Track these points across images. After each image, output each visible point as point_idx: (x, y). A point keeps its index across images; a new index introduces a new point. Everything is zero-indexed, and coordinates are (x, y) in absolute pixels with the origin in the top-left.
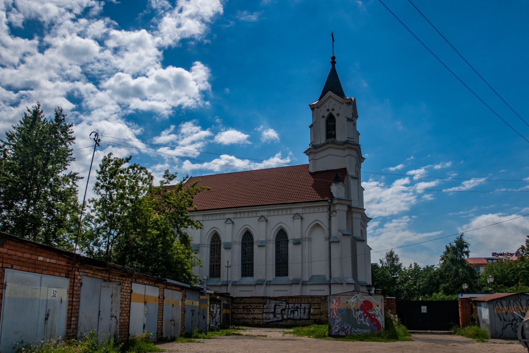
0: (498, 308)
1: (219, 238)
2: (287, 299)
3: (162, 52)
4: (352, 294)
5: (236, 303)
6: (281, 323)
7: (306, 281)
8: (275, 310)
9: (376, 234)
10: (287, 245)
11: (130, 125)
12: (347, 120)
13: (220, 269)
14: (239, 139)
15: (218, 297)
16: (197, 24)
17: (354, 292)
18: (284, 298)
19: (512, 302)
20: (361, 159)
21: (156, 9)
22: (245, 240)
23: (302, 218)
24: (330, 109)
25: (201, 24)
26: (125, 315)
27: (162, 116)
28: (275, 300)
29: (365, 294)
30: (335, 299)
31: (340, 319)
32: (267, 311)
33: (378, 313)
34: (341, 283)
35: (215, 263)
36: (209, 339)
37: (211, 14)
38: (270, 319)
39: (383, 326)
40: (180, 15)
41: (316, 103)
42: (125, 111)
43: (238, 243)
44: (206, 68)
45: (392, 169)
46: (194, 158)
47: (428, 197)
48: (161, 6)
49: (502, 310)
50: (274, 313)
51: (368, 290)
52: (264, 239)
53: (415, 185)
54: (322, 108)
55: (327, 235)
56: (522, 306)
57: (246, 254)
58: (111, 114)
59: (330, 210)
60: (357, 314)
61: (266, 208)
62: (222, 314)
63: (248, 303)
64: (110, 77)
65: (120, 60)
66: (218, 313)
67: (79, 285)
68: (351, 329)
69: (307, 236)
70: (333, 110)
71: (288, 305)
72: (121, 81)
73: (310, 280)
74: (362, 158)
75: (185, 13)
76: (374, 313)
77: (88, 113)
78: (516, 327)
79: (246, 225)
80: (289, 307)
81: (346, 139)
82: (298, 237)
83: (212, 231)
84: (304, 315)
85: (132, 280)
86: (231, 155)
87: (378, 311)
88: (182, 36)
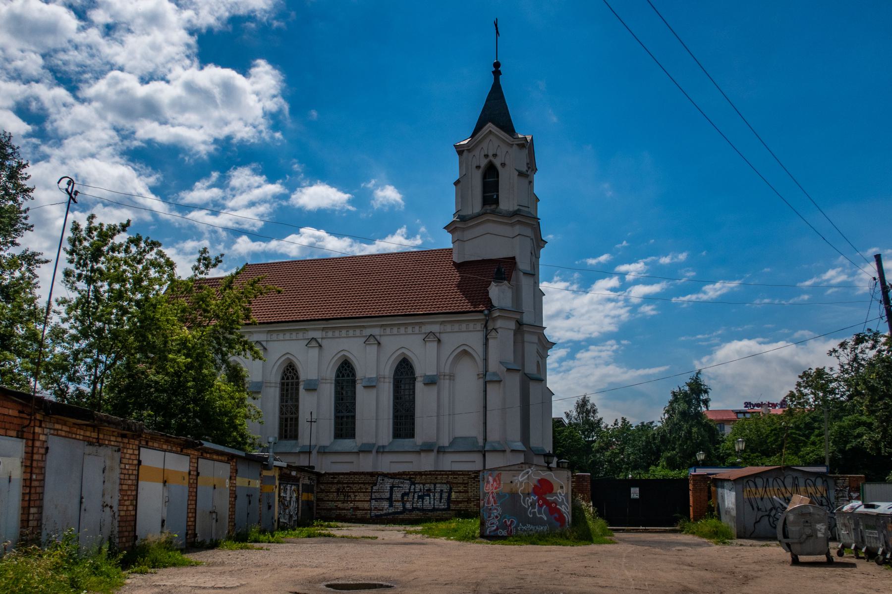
1: (296, 371)
2: (412, 477)
4: (520, 469)
5: (325, 483)
6: (401, 516)
8: (391, 494)
10: (414, 386)
12: (518, 175)
14: (334, 201)
15: (294, 473)
17: (523, 465)
18: (407, 475)
19: (771, 480)
22: (341, 376)
23: (439, 341)
24: (490, 154)
26: (127, 503)
27: (195, 154)
28: (391, 478)
29: (541, 469)
31: (499, 509)
32: (378, 496)
34: (503, 449)
35: (289, 415)
36: (278, 543)
38: (382, 510)
42: (127, 143)
43: (329, 381)
45: (592, 262)
49: (756, 493)
50: (390, 500)
53: (628, 290)
54: (477, 152)
55: (481, 369)
56: (786, 488)
57: (342, 399)
58: (101, 147)
59: (486, 328)
60: (528, 500)
62: (300, 502)
64: (97, 79)
66: (294, 499)
67: (42, 451)
68: (518, 525)
69: (447, 371)
70: (495, 155)
71: (413, 487)
76: (555, 499)
78: (775, 519)
80: (414, 489)
81: (516, 208)
82: (431, 372)
84: (440, 502)
85: (140, 443)
87: (561, 495)
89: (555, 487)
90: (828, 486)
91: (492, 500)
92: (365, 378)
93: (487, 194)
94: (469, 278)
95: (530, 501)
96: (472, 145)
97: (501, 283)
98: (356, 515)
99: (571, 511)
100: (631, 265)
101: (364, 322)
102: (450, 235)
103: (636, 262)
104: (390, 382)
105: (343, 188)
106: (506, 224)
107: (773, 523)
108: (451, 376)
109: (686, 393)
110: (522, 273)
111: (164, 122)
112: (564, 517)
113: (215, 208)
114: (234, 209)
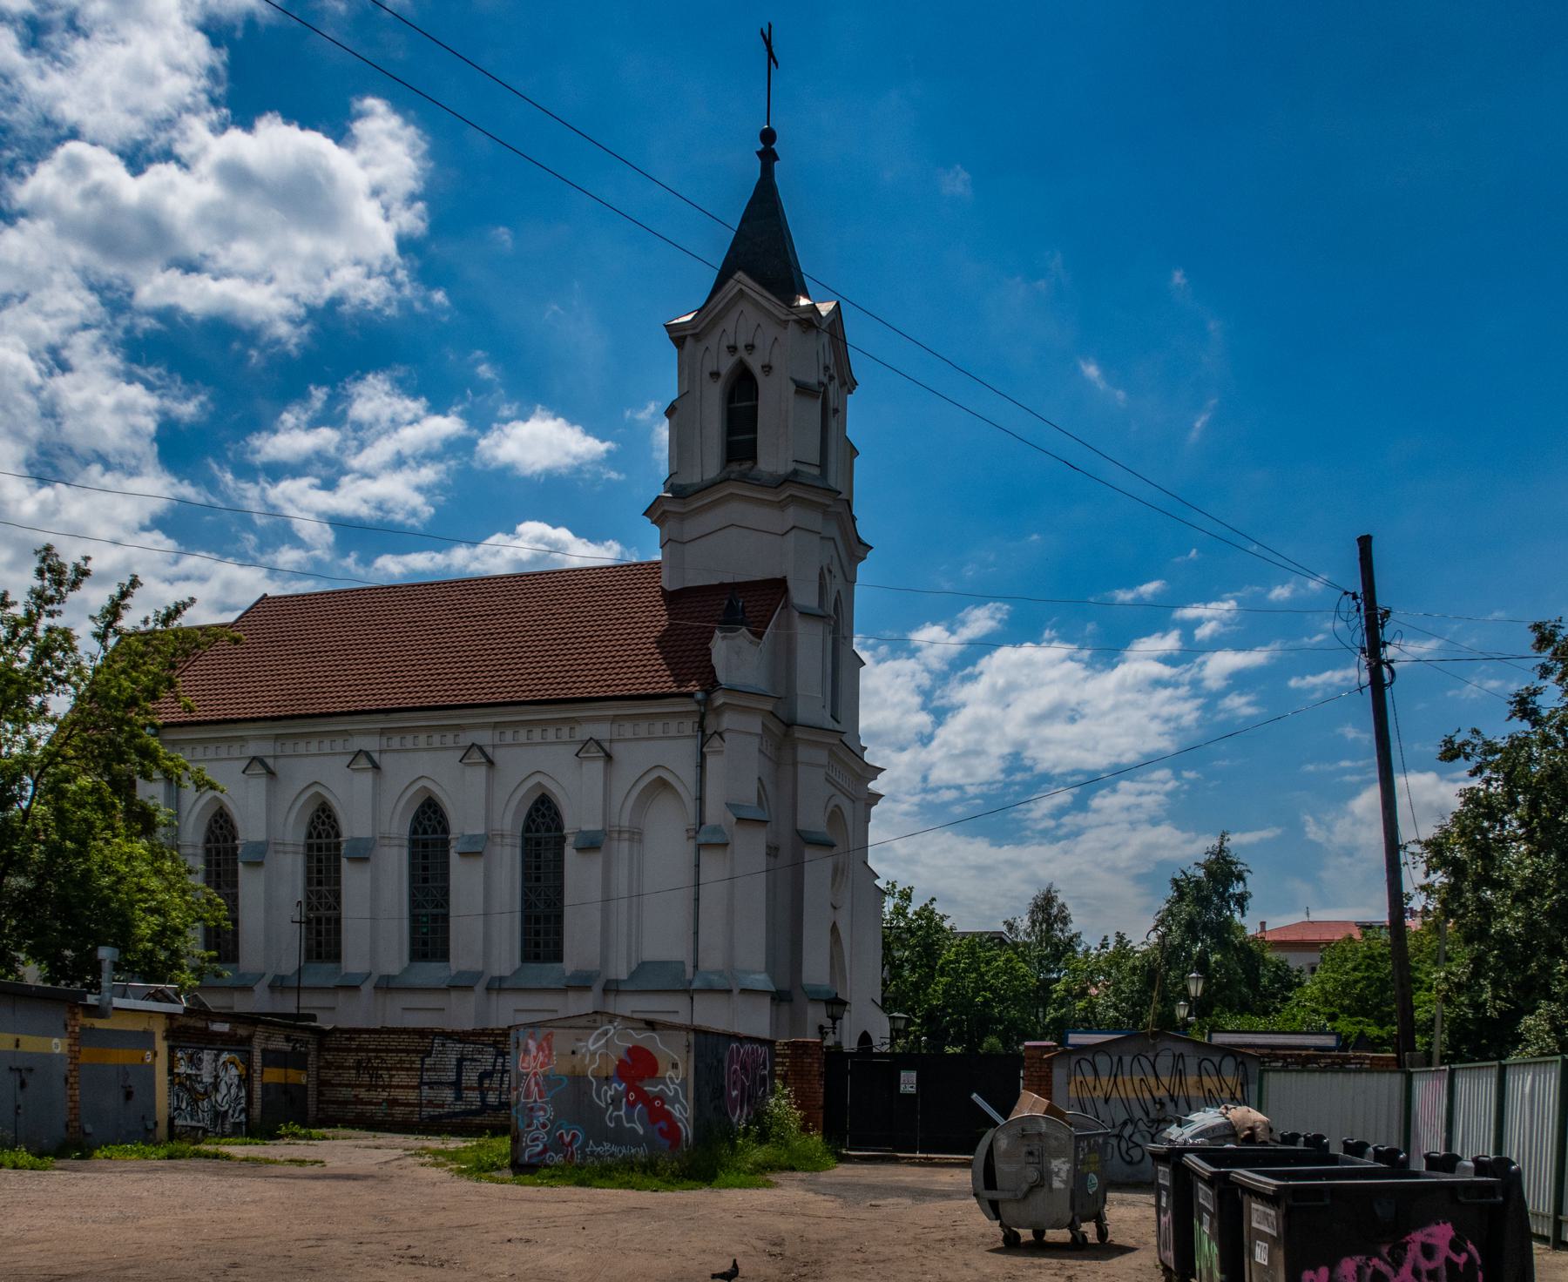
0: (1081, 1082)
1: (335, 821)
3: (224, 54)
6: (478, 1120)
7: (617, 981)
8: (459, 1074)
9: (1061, 832)
12: (796, 392)
13: (338, 932)
14: (575, 457)
17: (598, 1018)
18: (489, 1035)
19: (1127, 1060)
20: (858, 549)
23: (609, 757)
24: (741, 345)
30: (535, 1040)
31: (549, 1108)
33: (675, 1089)
34: (727, 987)
35: (323, 912)
36: (32, 1169)
38: (442, 1106)
39: (687, 1135)
41: (689, 318)
42: (124, 321)
43: (396, 842)
44: (411, 132)
45: (1124, 596)
46: (413, 526)
47: (1239, 705)
49: (1095, 1088)
50: (457, 1085)
52: (480, 831)
53: (1198, 660)
54: (712, 341)
55: (692, 820)
56: (1157, 1077)
57: (538, 879)
58: (72, 331)
59: (703, 732)
60: (606, 1092)
62: (257, 1087)
65: (57, 82)
68: (585, 1144)
69: (625, 823)
70: (750, 347)
71: (500, 1060)
72: (88, 183)
73: (633, 976)
76: (662, 1089)
78: (1131, 1145)
80: (503, 1065)
81: (791, 467)
82: (593, 824)
86: (555, 527)
87: (673, 1083)
89: (663, 1064)
90: (1246, 1075)
92: (463, 836)
93: (736, 438)
94: (690, 628)
95: (609, 1093)
96: (703, 325)
98: (392, 1115)
100: (1210, 606)
101: (460, 717)
102: (656, 530)
103: (1217, 598)
104: (513, 846)
107: (1127, 1153)
109: (1198, 883)
110: (797, 614)
111: (191, 267)
112: (678, 1127)
113: (329, 473)
114: (368, 475)
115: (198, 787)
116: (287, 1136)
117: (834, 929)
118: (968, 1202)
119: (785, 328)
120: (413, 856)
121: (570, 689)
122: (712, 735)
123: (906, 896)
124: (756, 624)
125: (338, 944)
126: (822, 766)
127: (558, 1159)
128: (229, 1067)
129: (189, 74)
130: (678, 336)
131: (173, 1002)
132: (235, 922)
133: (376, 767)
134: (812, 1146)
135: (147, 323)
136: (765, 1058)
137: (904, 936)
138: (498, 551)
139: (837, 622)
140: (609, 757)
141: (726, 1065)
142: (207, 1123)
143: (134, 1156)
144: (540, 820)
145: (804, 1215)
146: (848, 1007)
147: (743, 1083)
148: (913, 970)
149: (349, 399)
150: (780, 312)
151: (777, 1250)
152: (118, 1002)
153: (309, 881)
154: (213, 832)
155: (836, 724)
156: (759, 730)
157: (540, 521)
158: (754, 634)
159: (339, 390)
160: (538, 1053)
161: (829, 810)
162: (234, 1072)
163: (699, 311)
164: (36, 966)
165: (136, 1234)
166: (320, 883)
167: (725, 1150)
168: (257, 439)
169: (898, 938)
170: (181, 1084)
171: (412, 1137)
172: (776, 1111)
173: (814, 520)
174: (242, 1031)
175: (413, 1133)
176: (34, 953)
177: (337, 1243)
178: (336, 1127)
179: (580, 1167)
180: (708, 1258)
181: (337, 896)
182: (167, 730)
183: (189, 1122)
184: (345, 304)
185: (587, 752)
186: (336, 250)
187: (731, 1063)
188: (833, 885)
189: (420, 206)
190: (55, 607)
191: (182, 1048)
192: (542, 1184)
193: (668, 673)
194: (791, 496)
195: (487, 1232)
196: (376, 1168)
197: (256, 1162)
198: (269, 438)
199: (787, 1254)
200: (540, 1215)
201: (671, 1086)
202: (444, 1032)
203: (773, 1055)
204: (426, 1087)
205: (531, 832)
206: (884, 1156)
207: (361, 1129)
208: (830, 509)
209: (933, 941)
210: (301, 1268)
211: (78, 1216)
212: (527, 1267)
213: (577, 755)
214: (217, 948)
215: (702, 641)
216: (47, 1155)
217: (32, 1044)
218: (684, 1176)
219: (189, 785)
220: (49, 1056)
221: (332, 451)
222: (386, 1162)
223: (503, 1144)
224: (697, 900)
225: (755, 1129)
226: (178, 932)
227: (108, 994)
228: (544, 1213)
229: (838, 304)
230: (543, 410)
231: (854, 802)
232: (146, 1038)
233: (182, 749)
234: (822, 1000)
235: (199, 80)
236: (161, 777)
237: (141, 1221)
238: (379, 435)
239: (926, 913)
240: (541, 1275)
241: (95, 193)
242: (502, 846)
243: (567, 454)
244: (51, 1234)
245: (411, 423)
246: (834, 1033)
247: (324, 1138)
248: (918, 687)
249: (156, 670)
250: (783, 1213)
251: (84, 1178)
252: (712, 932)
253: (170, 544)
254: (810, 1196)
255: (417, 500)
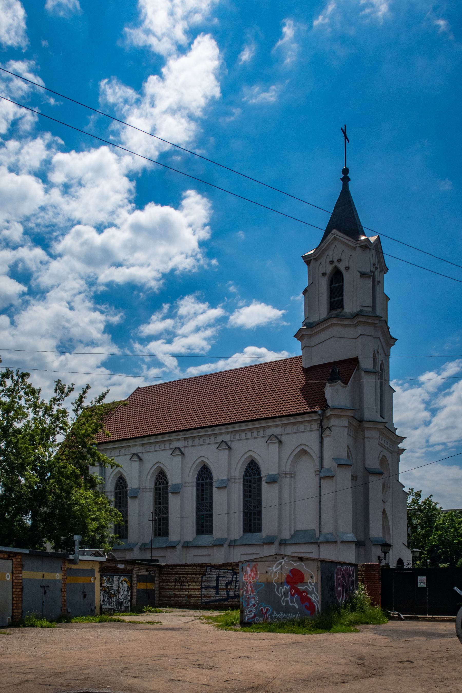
1: (166, 477)
3: (134, 183)
4: (274, 559)
5: (166, 574)
6: (225, 603)
7: (285, 540)
8: (217, 583)
11: (103, 309)
12: (361, 276)
14: (269, 318)
16: (182, 124)
17: (277, 556)
18: (230, 566)
21: (115, 105)
22: (158, 484)
23: (280, 442)
24: (335, 260)
25: (189, 123)
27: (148, 290)
28: (218, 569)
29: (293, 559)
31: (256, 598)
32: (207, 585)
34: (335, 540)
35: (161, 516)
36: (48, 627)
37: (202, 102)
38: (210, 597)
39: (318, 608)
40: (152, 110)
42: (93, 289)
43: (191, 484)
44: (205, 200)
46: (202, 354)
48: (121, 97)
50: (216, 588)
51: (383, 551)
52: (226, 477)
54: (323, 260)
55: (317, 467)
57: (250, 497)
58: (75, 295)
60: (281, 589)
61: (228, 428)
62: (135, 591)
63: (181, 574)
64: (63, 235)
65: (74, 204)
69: (288, 470)
70: (339, 260)
71: (235, 576)
72: (82, 240)
73: (292, 537)
74: (391, 337)
75: (162, 105)
76: (306, 588)
77: (41, 296)
79: (202, 456)
80: (236, 579)
81: (359, 309)
82: (273, 471)
83: (294, 457)
86: (260, 348)
87: (311, 585)
88: (160, 149)
89: (306, 577)
91: (250, 589)
95: (283, 590)
97: (334, 383)
98: (189, 601)
99: (320, 600)
101: (216, 430)
102: (299, 343)
104: (240, 483)
105: (276, 305)
106: (350, 326)
108: (291, 474)
110: (363, 372)
111: (119, 265)
112: (314, 605)
114: (185, 336)
115: (112, 466)
116: (146, 611)
117: (384, 512)
118: (454, 639)
119: (355, 250)
120: (197, 490)
121: (263, 414)
122: (326, 429)
123: (419, 495)
124: (345, 379)
125: (167, 529)
126: (377, 438)
127: (261, 620)
128: (124, 583)
129: (121, 193)
130: (308, 260)
131: (102, 556)
132: (126, 522)
133: (183, 454)
134: (376, 612)
135: (102, 288)
136: (353, 572)
137: (417, 513)
138: (237, 361)
139: (382, 374)
140: (280, 442)
141: (335, 576)
142: (114, 607)
143: (87, 621)
144: (251, 471)
145: (374, 645)
146: (391, 547)
147: (343, 584)
148: (422, 529)
149: (178, 307)
150: (352, 243)
151: (361, 662)
152: (81, 558)
153: (155, 503)
154: (118, 485)
155: (382, 419)
156: (347, 425)
157: (254, 346)
158: (344, 383)
159: (175, 304)
160: (251, 573)
161: (380, 458)
162: (126, 585)
163: (317, 248)
164: (49, 543)
165: (87, 655)
166: (160, 504)
167: (336, 615)
168: (142, 327)
169: (414, 514)
170: (105, 590)
171: (198, 611)
172: (359, 596)
173: (370, 330)
174: (129, 568)
175: (198, 609)
176: (49, 539)
177: (167, 658)
178: (166, 607)
179: (270, 624)
180: (329, 666)
181: (167, 508)
182: (101, 445)
183: (108, 607)
184: (177, 270)
185: (271, 441)
186: (174, 250)
187: (337, 575)
188: (383, 491)
189: (207, 228)
190: (61, 402)
191: (105, 576)
192: (253, 631)
193: (306, 403)
194: (359, 321)
195: (230, 654)
196: (183, 625)
197: (134, 623)
198: (147, 326)
199: (366, 664)
200: (253, 645)
201: (310, 586)
202: (211, 565)
203: (357, 570)
204: (204, 589)
205: (247, 476)
206: (413, 617)
207: (177, 608)
208: (377, 325)
209: (432, 514)
210: (152, 670)
211: (65, 647)
212: (248, 669)
213: (266, 442)
214: (119, 533)
215: (320, 388)
216: (54, 622)
217: (49, 576)
218: (317, 627)
219: (108, 466)
220: (55, 581)
221: (171, 328)
222: (187, 622)
223: (236, 614)
224: (320, 502)
225: (349, 605)
226: (103, 527)
227: (77, 554)
228: (255, 645)
229: (379, 236)
230: (256, 301)
231: (392, 453)
232: (91, 572)
233: (106, 452)
234: (379, 545)
235: (124, 194)
236: (98, 464)
237: (89, 649)
238: (190, 319)
239: (428, 502)
240: (254, 673)
241: (85, 243)
242: (285, 478)
243: (266, 318)
244: (55, 655)
245: (202, 313)
246: (385, 559)
247: (162, 612)
248: (423, 400)
249: (96, 421)
250: (363, 645)
251: (67, 631)
252: (327, 516)
253: (108, 372)
254: (376, 636)
255: (204, 344)
